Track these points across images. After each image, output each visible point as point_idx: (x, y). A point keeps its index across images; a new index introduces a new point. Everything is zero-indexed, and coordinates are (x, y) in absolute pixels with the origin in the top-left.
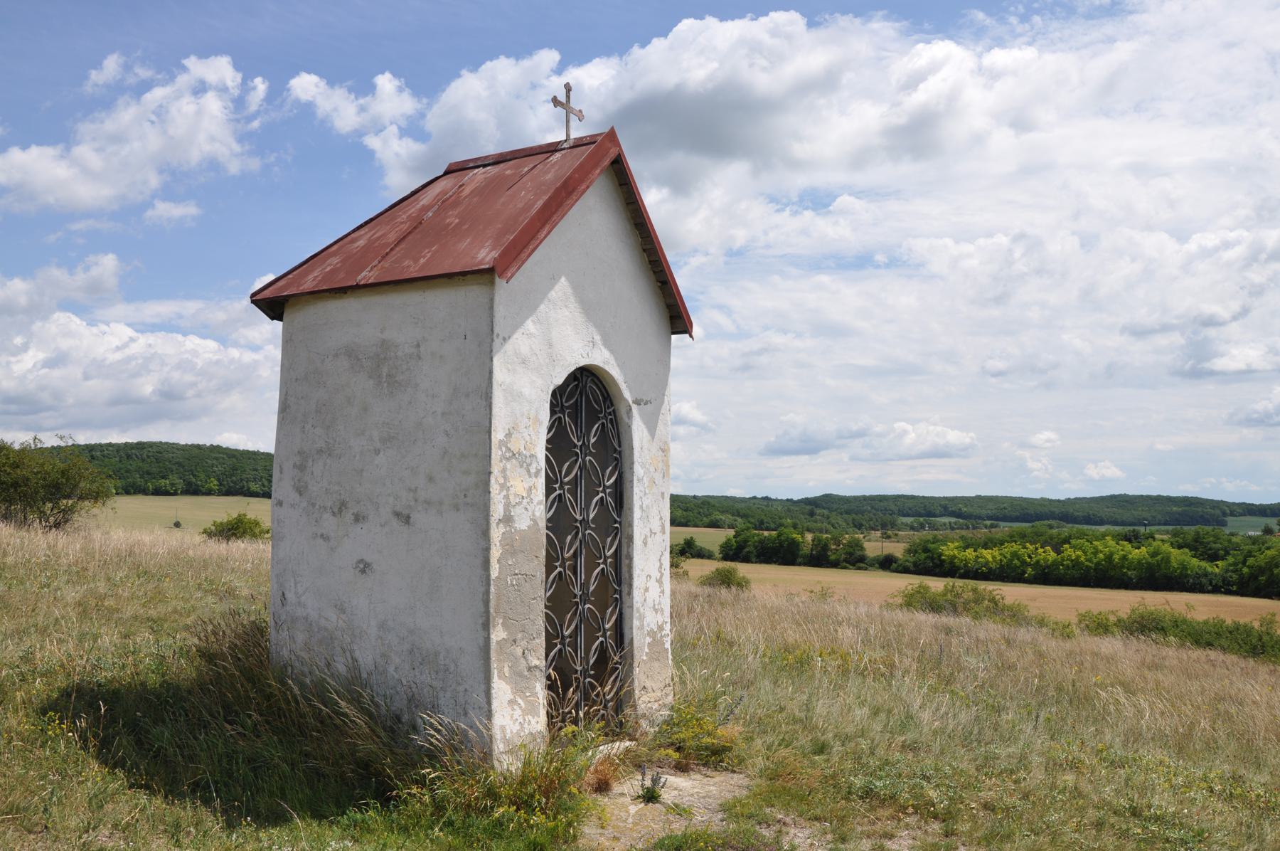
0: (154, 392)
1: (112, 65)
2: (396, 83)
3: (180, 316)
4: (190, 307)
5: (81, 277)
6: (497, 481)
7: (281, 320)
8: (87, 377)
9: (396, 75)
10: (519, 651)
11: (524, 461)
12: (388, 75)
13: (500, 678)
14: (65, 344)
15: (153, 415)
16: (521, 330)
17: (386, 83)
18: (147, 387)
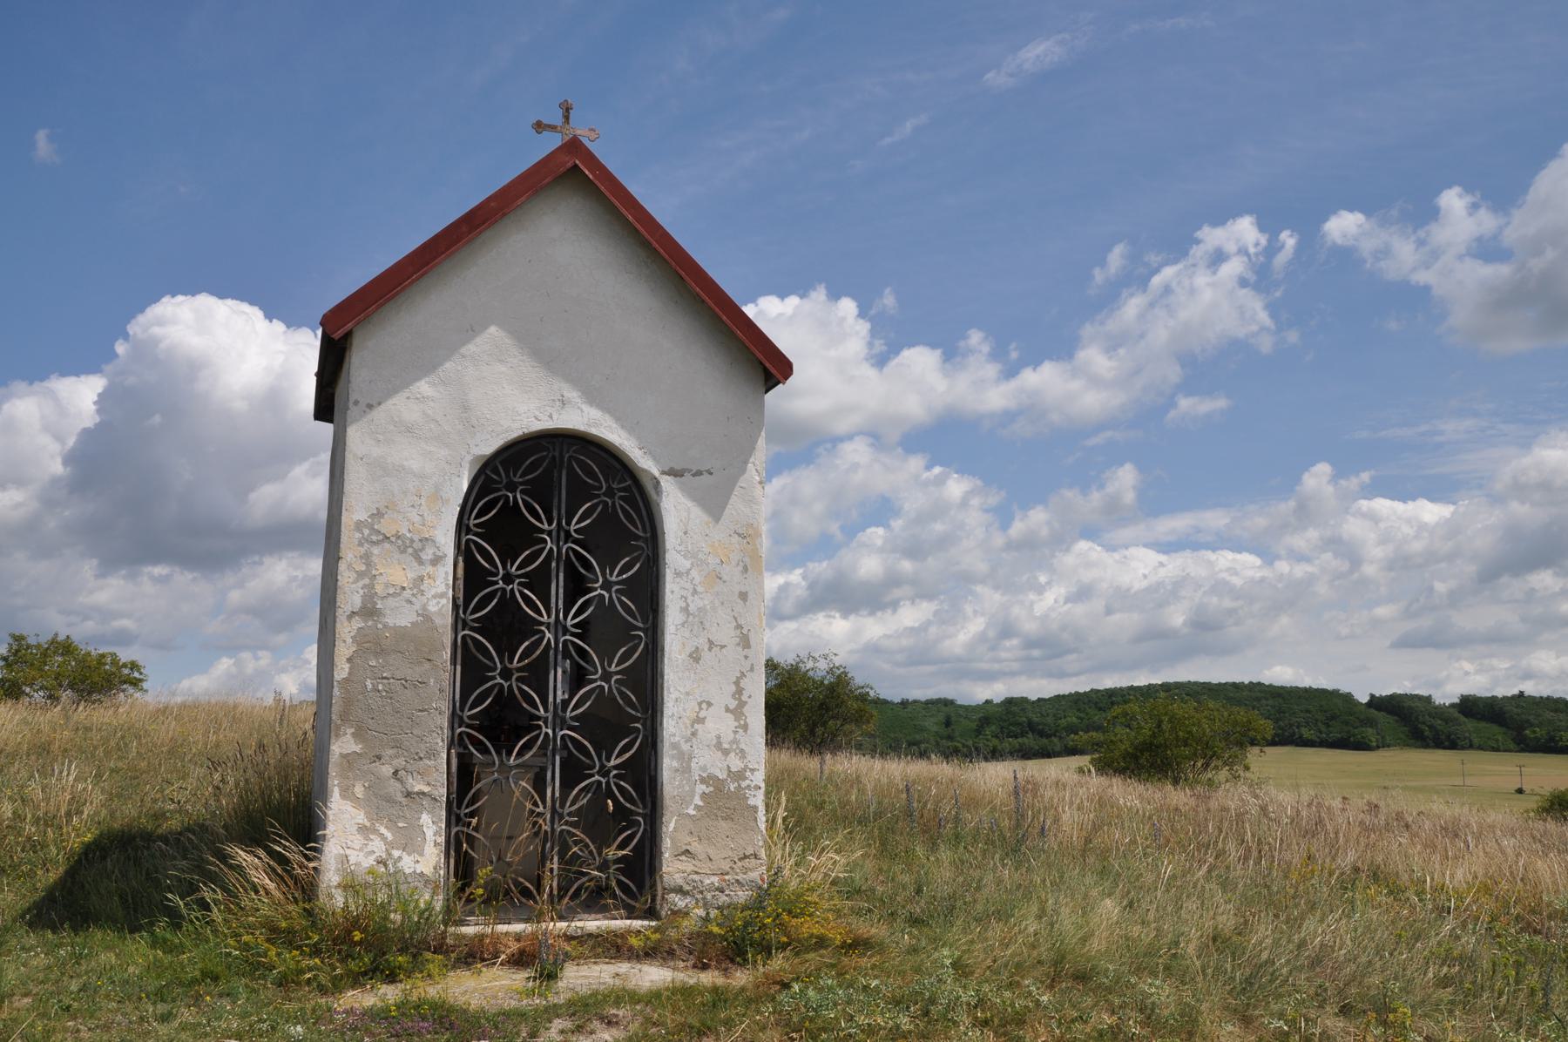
0: (1185, 624)
1: (1116, 257)
2: (1469, 199)
3: (1198, 530)
4: (1216, 519)
5: (1096, 497)
6: (350, 566)
7: (331, 421)
8: (1109, 611)
9: (1468, 189)
10: (387, 770)
11: (414, 548)
12: (1457, 190)
13: (343, 797)
14: (1087, 576)
15: (1187, 650)
16: (406, 393)
17: (1453, 201)
18: (1177, 617)
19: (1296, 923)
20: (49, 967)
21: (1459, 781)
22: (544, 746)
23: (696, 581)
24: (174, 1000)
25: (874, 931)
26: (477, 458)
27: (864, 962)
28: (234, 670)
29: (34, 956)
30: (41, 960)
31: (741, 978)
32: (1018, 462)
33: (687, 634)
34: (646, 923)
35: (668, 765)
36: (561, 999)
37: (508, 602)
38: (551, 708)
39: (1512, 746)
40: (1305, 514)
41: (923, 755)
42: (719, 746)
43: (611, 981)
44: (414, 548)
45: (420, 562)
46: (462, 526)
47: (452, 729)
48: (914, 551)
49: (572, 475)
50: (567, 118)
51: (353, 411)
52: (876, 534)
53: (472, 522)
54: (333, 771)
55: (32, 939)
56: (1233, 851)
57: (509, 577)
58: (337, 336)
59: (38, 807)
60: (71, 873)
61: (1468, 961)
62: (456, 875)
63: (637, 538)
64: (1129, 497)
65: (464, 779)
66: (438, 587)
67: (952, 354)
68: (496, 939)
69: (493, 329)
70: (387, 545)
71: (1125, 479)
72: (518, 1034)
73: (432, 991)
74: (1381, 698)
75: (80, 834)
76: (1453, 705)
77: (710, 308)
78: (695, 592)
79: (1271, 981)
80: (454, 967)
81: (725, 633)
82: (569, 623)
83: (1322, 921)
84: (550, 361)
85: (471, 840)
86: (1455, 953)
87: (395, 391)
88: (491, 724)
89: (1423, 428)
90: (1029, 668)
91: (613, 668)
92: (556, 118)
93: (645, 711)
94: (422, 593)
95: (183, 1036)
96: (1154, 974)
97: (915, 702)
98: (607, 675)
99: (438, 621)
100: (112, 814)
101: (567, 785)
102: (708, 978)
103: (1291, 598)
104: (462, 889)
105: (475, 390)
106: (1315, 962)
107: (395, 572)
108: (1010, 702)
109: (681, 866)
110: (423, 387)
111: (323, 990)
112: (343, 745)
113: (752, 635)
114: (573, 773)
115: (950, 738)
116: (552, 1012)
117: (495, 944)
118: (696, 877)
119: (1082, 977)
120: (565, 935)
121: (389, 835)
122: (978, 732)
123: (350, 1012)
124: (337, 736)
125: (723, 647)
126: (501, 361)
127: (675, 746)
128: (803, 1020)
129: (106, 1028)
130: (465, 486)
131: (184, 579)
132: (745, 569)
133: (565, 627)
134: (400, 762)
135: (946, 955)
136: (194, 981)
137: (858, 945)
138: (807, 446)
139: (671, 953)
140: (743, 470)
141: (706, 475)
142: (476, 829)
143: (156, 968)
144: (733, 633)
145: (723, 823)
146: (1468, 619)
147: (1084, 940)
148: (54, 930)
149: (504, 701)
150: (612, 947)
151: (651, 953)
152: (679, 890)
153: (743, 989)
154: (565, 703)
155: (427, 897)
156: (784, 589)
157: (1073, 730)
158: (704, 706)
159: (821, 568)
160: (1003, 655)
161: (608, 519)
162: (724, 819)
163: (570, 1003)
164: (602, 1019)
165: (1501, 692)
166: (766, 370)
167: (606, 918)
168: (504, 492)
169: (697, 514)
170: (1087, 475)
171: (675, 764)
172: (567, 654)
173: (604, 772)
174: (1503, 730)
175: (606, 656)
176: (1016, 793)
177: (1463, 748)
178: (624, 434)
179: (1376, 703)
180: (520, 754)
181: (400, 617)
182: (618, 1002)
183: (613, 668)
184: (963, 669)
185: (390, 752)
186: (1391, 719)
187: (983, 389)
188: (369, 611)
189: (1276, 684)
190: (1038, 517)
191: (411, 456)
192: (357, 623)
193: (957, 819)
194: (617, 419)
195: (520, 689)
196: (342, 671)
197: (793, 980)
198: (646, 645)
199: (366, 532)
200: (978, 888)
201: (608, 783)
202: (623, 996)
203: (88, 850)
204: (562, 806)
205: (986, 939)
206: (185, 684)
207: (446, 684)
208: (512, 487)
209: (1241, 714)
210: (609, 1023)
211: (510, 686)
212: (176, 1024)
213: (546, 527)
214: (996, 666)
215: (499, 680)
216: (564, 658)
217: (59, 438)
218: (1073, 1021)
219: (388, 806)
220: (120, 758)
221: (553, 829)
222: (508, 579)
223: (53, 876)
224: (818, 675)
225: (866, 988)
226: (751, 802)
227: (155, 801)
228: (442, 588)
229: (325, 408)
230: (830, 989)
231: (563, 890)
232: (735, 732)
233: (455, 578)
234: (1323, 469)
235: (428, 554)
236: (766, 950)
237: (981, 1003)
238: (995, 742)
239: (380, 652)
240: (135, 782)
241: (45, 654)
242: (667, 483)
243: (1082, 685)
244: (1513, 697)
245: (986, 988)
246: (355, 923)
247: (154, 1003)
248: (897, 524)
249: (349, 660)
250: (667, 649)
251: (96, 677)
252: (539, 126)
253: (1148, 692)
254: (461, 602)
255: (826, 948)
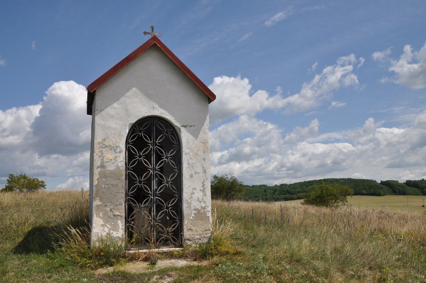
3: (329, 138)
7: (91, 115)
8: (310, 160)
10: (108, 209)
11: (114, 149)
13: (97, 217)
15: (331, 170)
18: (329, 161)
19: (357, 245)
20: (19, 264)
21: (406, 204)
22: (151, 201)
23: (191, 156)
24: (52, 272)
25: (242, 249)
26: (131, 124)
27: (239, 258)
28: (74, 182)
29: (14, 262)
30: (17, 262)
31: (205, 263)
32: (288, 121)
33: (189, 170)
34: (179, 249)
35: (185, 206)
36: (156, 270)
37: (140, 163)
38: (153, 191)
39: (421, 194)
40: (366, 132)
41: (258, 200)
42: (198, 200)
43: (170, 265)
44: (114, 149)
45: (116, 152)
46: (127, 142)
47: (126, 197)
48: (259, 145)
49: (156, 127)
50: (153, 30)
51: (97, 112)
52: (248, 140)
53: (130, 141)
54: (94, 210)
55: (15, 257)
56: (341, 225)
57: (140, 156)
58: (91, 92)
59: (16, 221)
60: (25, 239)
61: (404, 254)
62: (128, 237)
63: (175, 144)
64: (316, 129)
65: (130, 210)
66: (121, 159)
67: (272, 93)
68: (139, 254)
69: (134, 89)
70: (107, 148)
71: (315, 124)
72: (145, 280)
73: (122, 269)
74: (384, 182)
75: (27, 229)
76: (404, 183)
77: (193, 81)
78: (191, 159)
79: (350, 261)
80: (128, 262)
81: (199, 170)
82: (157, 168)
83: (365, 243)
84: (150, 97)
85: (132, 228)
86: (401, 252)
87: (108, 106)
88: (136, 196)
89: (389, 110)
90: (288, 176)
91: (169, 180)
92: (150, 31)
93: (178, 191)
94: (117, 161)
95: (54, 282)
96: (318, 259)
97: (256, 186)
98: (168, 181)
99: (121, 168)
100: (36, 222)
101: (158, 212)
102: (195, 263)
103: (361, 155)
104: (129, 241)
105: (130, 105)
106: (363, 255)
107: (109, 155)
108: (282, 185)
109: (189, 233)
110: (115, 105)
111: (93, 269)
112: (96, 203)
113: (207, 170)
114: (159, 208)
115: (266, 195)
116: (154, 273)
117: (139, 256)
118: (193, 236)
119: (298, 261)
120: (158, 252)
121: (109, 226)
122: (274, 193)
123: (99, 275)
124: (95, 200)
125: (199, 173)
126: (136, 97)
127: (186, 200)
128: (221, 274)
129: (34, 280)
130: (128, 132)
131: (62, 158)
132: (204, 152)
133: (156, 169)
134: (112, 207)
135: (261, 256)
136: (58, 267)
137: (237, 253)
138: (229, 116)
139: (187, 257)
140: (203, 125)
141: (193, 127)
142: (133, 224)
143: (48, 264)
144: (201, 169)
145: (200, 221)
146: (412, 159)
147: (299, 251)
148: (20, 254)
149: (140, 190)
150: (171, 255)
151: (181, 256)
152: (189, 240)
153: (206, 266)
154: (156, 190)
155: (120, 243)
156: (222, 156)
157: (299, 192)
158: (194, 189)
159: (233, 150)
160: (281, 173)
161: (167, 139)
162: (200, 220)
163: (159, 271)
164: (167, 275)
165: (417, 179)
166: (209, 98)
167: (169, 247)
168: (138, 133)
169: (191, 137)
170: (306, 123)
171: (186, 205)
172: (156, 176)
173: (167, 208)
174: (418, 189)
175: (167, 177)
176: (281, 211)
177: (407, 195)
178: (170, 116)
179: (382, 183)
180: (145, 203)
181: (111, 167)
182: (172, 270)
183: (169, 180)
184: (271, 176)
185: (109, 204)
186: (387, 187)
187: (278, 102)
188: (102, 166)
189: (355, 178)
190: (293, 135)
191: (113, 124)
192: (99, 169)
193: (265, 218)
194: (169, 112)
195: (144, 186)
196: (95, 183)
197: (219, 263)
198: (178, 173)
199: (101, 145)
200: (271, 237)
201: (168, 211)
202: (175, 269)
203: (30, 232)
204: (156, 217)
205: (273, 251)
206: (59, 186)
207: (124, 185)
208: (140, 131)
209: (345, 187)
210: (169, 276)
211: (141, 186)
212: (52, 279)
213: (150, 142)
214: (280, 176)
215: (138, 184)
216: (156, 177)
217: (29, 120)
218: (295, 273)
219: (109, 219)
220: (39, 207)
221: (154, 224)
222: (140, 156)
223: (21, 239)
224: (228, 180)
225: (239, 265)
226: (208, 215)
227: (48, 218)
228: (122, 159)
229: (90, 110)
230: (229, 266)
231: (157, 240)
232: (203, 196)
233: (126, 157)
234: (371, 120)
235: (118, 150)
236: (212, 256)
237: (270, 269)
238: (278, 196)
239: (106, 177)
240: (43, 213)
241: (19, 179)
242: (183, 129)
243: (302, 180)
244: (421, 180)
245: (272, 264)
246: (101, 251)
247: (47, 273)
248: (255, 137)
249: (97, 180)
250: (184, 174)
251: (33, 185)
252: (145, 33)
253: (320, 181)
254: (127, 163)
255: (229, 254)
